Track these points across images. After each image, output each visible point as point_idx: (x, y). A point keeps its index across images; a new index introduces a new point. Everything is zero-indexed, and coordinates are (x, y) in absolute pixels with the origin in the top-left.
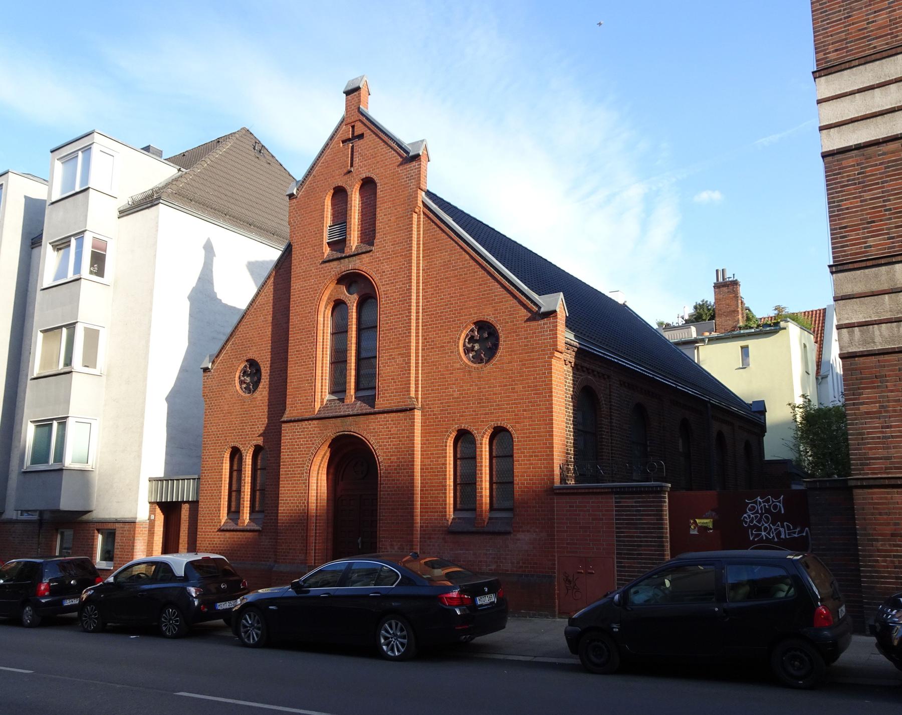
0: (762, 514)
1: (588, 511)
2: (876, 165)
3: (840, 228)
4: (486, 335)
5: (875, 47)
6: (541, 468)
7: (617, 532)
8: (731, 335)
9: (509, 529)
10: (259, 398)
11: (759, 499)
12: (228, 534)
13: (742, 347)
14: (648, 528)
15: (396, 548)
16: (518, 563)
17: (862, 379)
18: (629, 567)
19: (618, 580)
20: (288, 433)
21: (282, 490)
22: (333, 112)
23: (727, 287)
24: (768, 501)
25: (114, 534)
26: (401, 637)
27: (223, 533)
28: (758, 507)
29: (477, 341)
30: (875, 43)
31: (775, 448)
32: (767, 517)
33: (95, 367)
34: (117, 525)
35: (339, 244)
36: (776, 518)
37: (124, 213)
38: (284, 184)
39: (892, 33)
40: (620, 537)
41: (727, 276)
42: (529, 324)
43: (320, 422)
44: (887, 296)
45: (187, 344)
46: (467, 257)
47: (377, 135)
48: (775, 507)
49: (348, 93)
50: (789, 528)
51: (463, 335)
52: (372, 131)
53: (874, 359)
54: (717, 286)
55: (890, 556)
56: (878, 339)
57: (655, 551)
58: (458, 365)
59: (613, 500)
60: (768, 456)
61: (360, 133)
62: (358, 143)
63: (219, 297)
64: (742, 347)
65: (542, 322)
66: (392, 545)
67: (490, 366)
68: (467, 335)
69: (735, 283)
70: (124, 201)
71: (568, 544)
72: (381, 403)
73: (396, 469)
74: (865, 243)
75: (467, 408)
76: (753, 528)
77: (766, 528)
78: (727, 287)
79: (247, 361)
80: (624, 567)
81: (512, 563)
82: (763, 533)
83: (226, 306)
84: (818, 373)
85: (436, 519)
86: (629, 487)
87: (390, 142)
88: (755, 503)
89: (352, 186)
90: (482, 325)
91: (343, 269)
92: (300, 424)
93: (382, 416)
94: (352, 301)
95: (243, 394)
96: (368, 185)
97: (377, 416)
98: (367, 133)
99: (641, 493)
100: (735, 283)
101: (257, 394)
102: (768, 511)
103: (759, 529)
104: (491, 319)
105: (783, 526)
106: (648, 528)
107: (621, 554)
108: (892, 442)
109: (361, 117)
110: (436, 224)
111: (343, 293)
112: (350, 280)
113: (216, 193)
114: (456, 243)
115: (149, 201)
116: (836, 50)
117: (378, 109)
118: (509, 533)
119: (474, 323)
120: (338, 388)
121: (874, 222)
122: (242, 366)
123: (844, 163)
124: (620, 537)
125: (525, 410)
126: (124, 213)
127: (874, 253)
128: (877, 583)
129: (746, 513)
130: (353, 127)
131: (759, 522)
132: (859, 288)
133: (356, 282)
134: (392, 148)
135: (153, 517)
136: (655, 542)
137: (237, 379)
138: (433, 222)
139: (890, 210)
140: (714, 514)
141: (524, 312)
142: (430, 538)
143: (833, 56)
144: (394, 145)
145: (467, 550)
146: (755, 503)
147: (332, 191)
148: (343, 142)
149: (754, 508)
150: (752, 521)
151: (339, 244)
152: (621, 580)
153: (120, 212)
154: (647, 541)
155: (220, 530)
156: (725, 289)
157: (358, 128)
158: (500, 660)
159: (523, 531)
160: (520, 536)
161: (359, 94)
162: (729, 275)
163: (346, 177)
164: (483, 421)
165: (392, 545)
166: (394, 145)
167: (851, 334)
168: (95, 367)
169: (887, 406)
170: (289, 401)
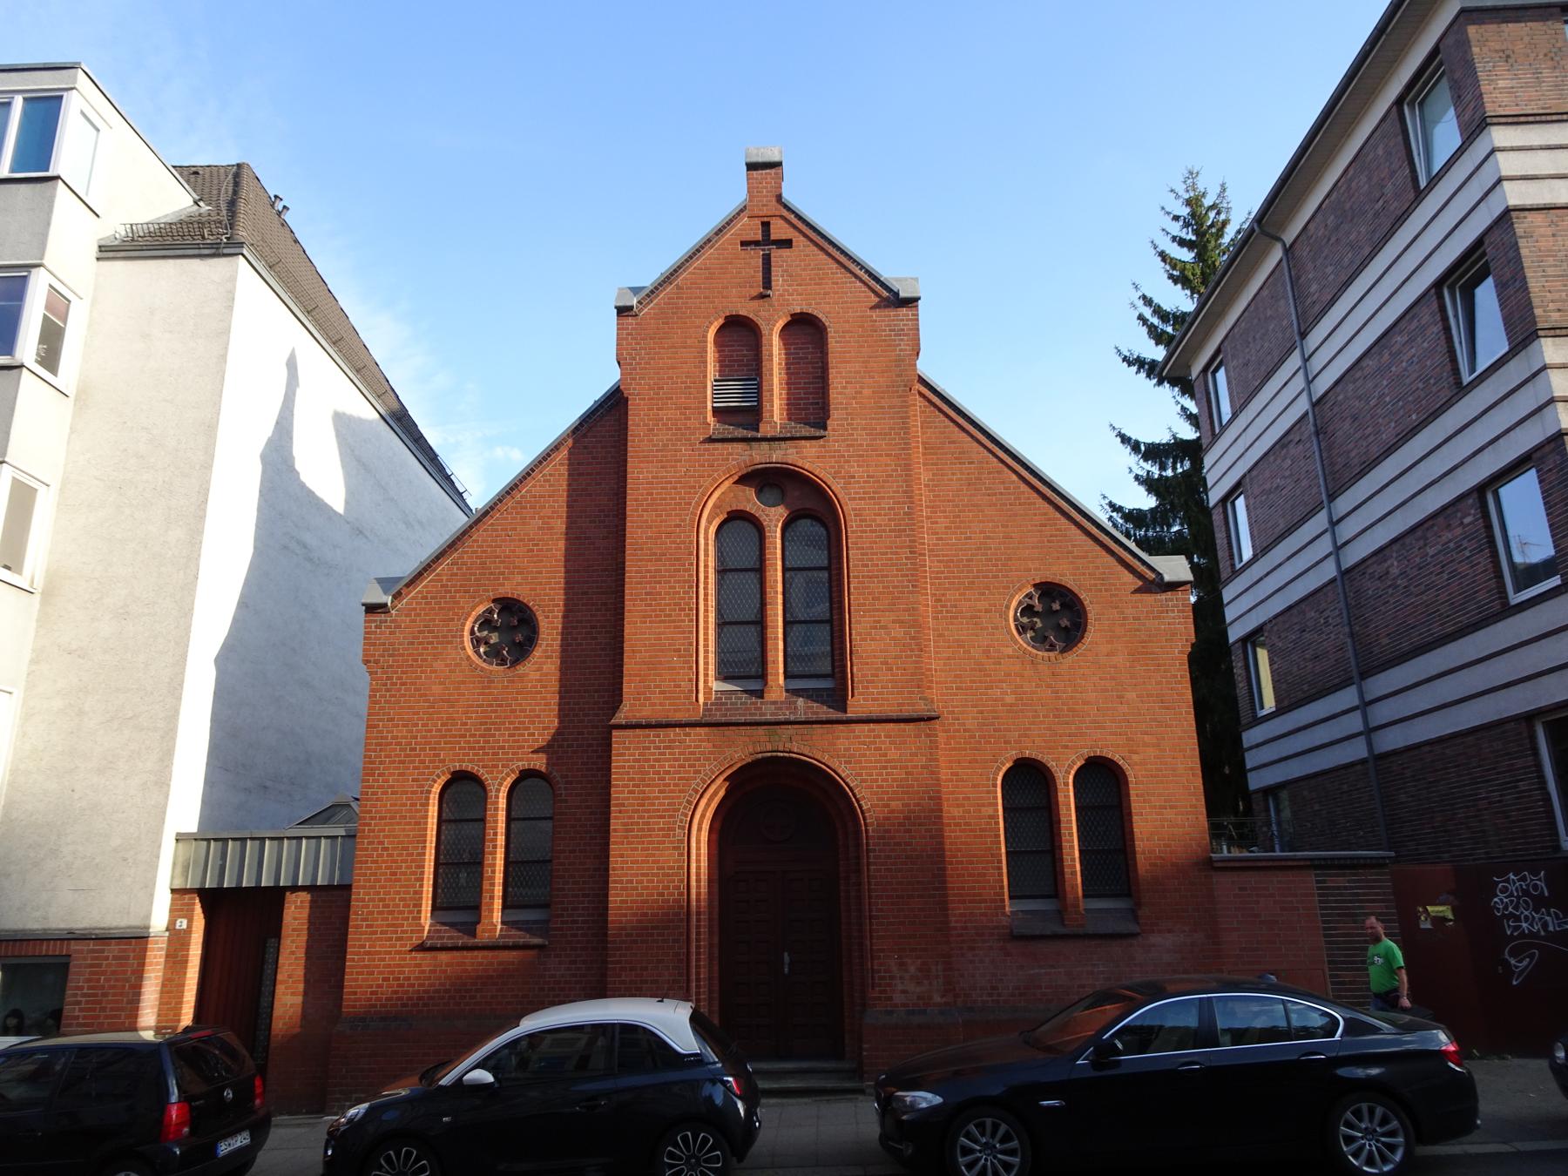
0: (1518, 898)
4: (1056, 606)
9: (1135, 928)
10: (534, 676)
12: (444, 957)
15: (912, 969)
18: (1351, 983)
20: (627, 751)
21: (615, 862)
22: (733, 192)
24: (1523, 879)
25: (66, 966)
26: (1004, 1152)
27: (428, 955)
29: (1037, 614)
33: (19, 572)
34: (74, 946)
35: (743, 418)
36: (1539, 903)
37: (108, 252)
42: (1138, 596)
43: (715, 730)
45: (251, 550)
46: (1014, 477)
47: (822, 249)
48: (1536, 887)
51: (1014, 604)
52: (811, 240)
58: (1009, 651)
59: (1310, 879)
62: (778, 255)
63: (298, 466)
65: (1163, 596)
66: (902, 965)
67: (1070, 658)
68: (1020, 603)
70: (114, 226)
72: (858, 704)
73: (900, 824)
77: (1527, 918)
79: (494, 601)
80: (1343, 983)
83: (303, 486)
85: (984, 915)
86: (1332, 859)
87: (852, 267)
88: (1507, 881)
89: (771, 322)
90: (1048, 590)
91: (758, 459)
92: (662, 732)
93: (866, 727)
94: (774, 518)
95: (484, 665)
96: (805, 328)
97: (853, 726)
98: (799, 240)
99: (1364, 866)
101: (527, 668)
102: (1526, 893)
103: (1517, 919)
104: (1069, 581)
109: (785, 213)
110: (947, 416)
111: (749, 500)
112: (767, 480)
114: (990, 451)
118: (1133, 935)
119: (1035, 586)
120: (742, 666)
122: (481, 609)
126: (108, 252)
128: (698, 894)
131: (1516, 908)
134: (856, 276)
135: (182, 924)
137: (466, 633)
138: (940, 410)
140: (1451, 898)
141: (1128, 577)
142: (973, 949)
144: (861, 273)
145: (1052, 967)
146: (1507, 881)
147: (721, 321)
148: (743, 244)
150: (1506, 908)
151: (743, 418)
153: (101, 248)
155: (422, 948)
157: (770, 230)
160: (1155, 939)
163: (756, 303)
164: (1066, 747)
166: (861, 273)
168: (19, 572)
170: (628, 688)
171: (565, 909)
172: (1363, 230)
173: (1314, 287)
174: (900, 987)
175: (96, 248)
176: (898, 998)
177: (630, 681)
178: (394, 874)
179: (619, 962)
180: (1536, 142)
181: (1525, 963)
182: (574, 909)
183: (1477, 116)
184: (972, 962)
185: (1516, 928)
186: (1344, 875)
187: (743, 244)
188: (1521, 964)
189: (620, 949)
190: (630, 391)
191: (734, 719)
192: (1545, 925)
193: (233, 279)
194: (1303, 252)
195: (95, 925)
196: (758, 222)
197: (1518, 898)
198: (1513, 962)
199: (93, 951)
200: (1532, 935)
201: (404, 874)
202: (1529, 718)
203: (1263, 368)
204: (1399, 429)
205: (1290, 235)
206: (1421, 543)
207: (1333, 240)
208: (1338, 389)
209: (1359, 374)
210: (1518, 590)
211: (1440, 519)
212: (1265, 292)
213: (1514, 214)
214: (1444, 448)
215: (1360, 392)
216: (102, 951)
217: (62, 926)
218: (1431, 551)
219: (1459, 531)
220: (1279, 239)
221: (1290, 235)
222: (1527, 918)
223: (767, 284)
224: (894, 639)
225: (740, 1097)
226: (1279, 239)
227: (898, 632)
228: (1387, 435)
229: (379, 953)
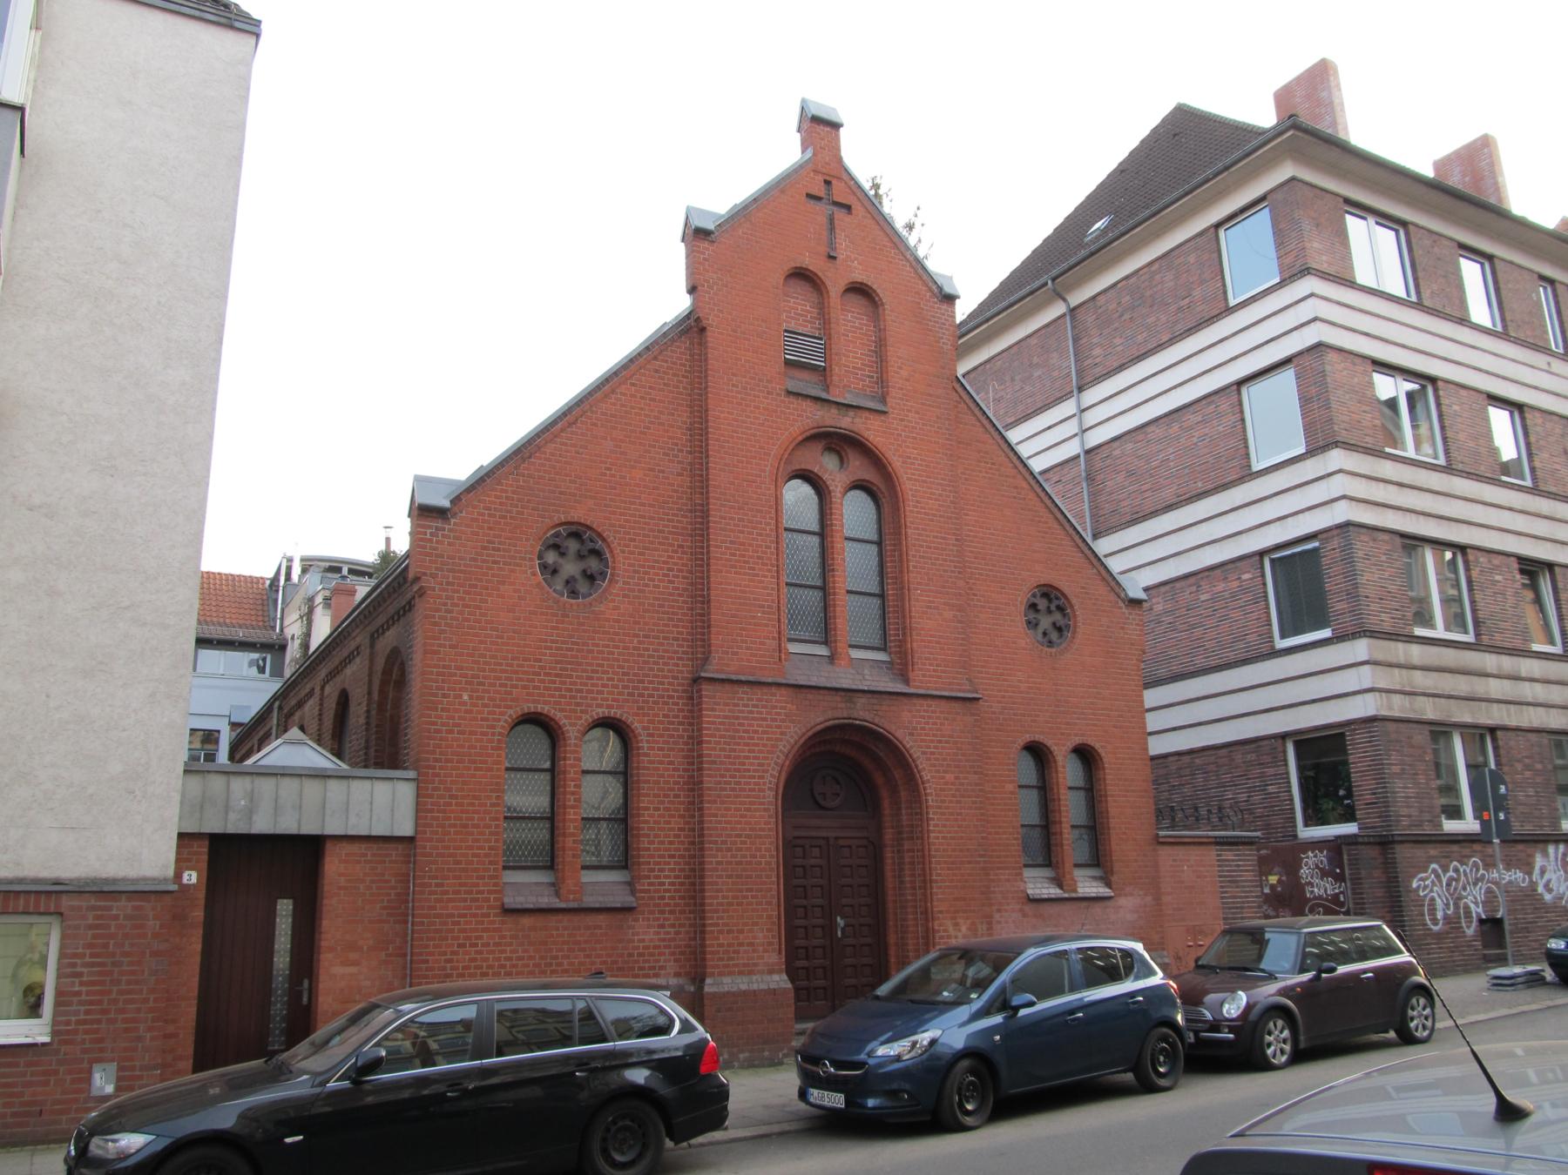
15: (964, 929)
59: (1211, 854)
142: (999, 911)
160: (1122, 901)
165: (957, 924)
171: (653, 870)
172: (1163, 318)
173: (1097, 351)
177: (718, 633)
178: (466, 826)
179: (717, 925)
180: (1335, 297)
182: (661, 870)
183: (1299, 263)
187: (808, 195)
189: (717, 911)
190: (711, 321)
191: (763, 680)
194: (1089, 318)
195: (92, 874)
196: (820, 178)
199: (93, 908)
200: (1320, 897)
201: (478, 826)
202: (1283, 737)
203: (1021, 408)
204: (1180, 491)
205: (1076, 298)
206: (1194, 589)
207: (1127, 316)
208: (1117, 444)
209: (1140, 437)
210: (1283, 637)
211: (1218, 572)
212: (1034, 341)
213: (1331, 356)
215: (1140, 453)
216: (109, 908)
217: (45, 874)
218: (1203, 598)
219: (1236, 584)
220: (1064, 300)
221: (1076, 298)
225: (1317, 978)
226: (1064, 300)
227: (948, 614)
228: (1168, 494)
229: (452, 915)
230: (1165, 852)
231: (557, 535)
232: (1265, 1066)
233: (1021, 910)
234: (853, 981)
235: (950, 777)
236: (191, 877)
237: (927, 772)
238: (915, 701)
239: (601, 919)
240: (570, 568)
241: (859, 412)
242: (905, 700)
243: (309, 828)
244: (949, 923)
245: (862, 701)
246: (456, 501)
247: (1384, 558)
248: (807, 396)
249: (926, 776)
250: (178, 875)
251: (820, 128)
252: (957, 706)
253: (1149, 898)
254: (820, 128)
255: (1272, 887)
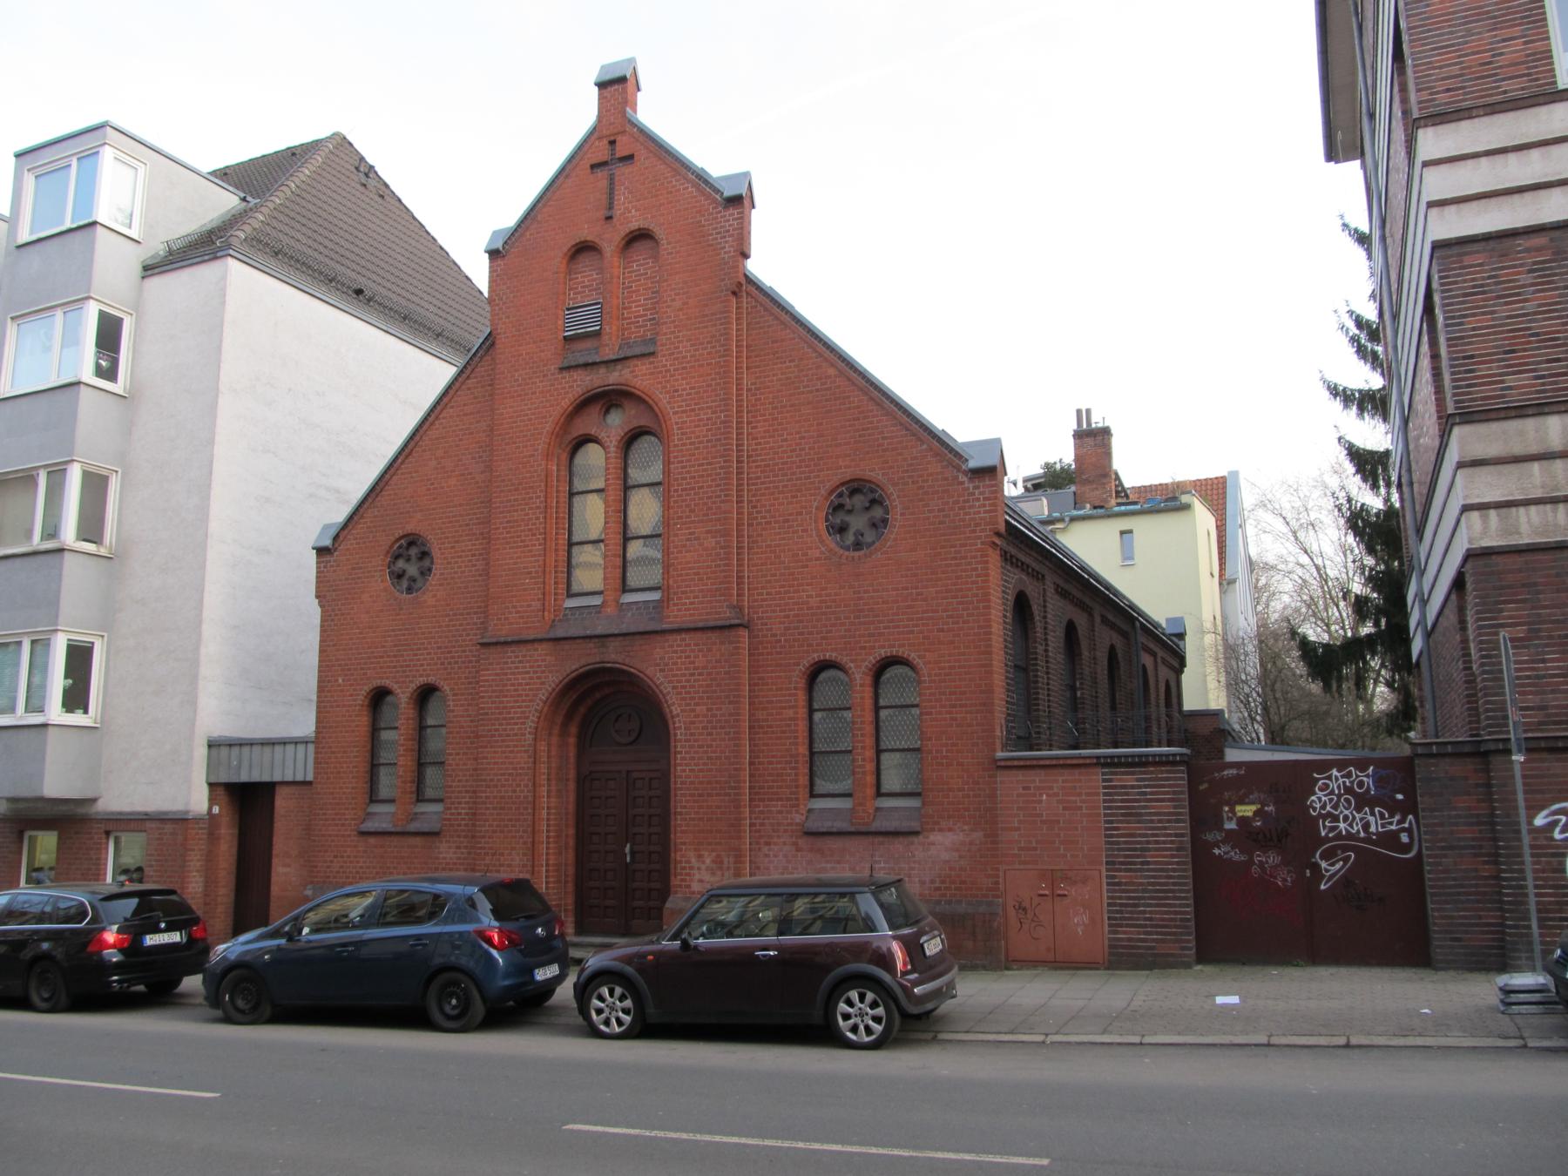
1: (1057, 795)
2: (1515, 266)
3: (1465, 358)
5: (1505, 92)
6: (970, 725)
7: (1107, 829)
8: (1101, 512)
9: (915, 825)
11: (1334, 772)
13: (1122, 533)
14: (1160, 821)
15: (708, 861)
16: (932, 882)
17: (1502, 588)
19: (1109, 905)
23: (1093, 440)
24: (1349, 775)
28: (1333, 785)
30: (1505, 85)
31: (1203, 688)
32: (1347, 800)
36: (1363, 801)
38: (275, 223)
39: (1529, 75)
40: (1112, 836)
41: (1094, 419)
44: (1536, 466)
48: (1361, 784)
49: (602, 85)
50: (1382, 816)
53: (1520, 560)
54: (1079, 436)
55: (1545, 855)
56: (1524, 528)
57: (1173, 856)
58: (815, 553)
59: (1097, 777)
60: (1190, 703)
61: (626, 153)
62: (623, 171)
64: (1122, 533)
66: (700, 856)
69: (1105, 433)
71: (1020, 849)
74: (1502, 382)
75: (834, 625)
76: (1325, 817)
77: (1346, 818)
78: (1093, 440)
80: (1119, 884)
81: (922, 883)
82: (1342, 825)
84: (1221, 576)
88: (1329, 778)
91: (597, 383)
100: (1105, 433)
102: (1349, 790)
103: (1336, 819)
105: (1373, 814)
106: (1160, 821)
107: (1113, 863)
108: (1548, 684)
113: (310, 242)
115: (205, 246)
116: (1448, 90)
117: (650, 112)
118: (916, 833)
121: (1513, 351)
123: (1467, 260)
124: (1112, 836)
125: (942, 630)
127: (1515, 399)
129: (1314, 793)
130: (612, 143)
131: (1335, 807)
132: (1493, 451)
133: (617, 406)
136: (1172, 842)
139: (1537, 335)
142: (768, 844)
143: (1442, 98)
146: (1329, 778)
149: (1327, 786)
150: (1323, 807)
152: (1115, 905)
154: (1157, 842)
156: (1090, 441)
157: (618, 148)
158: (950, 1041)
159: (941, 830)
160: (935, 837)
161: (625, 91)
162: (1097, 421)
165: (700, 856)
167: (1485, 519)
169: (1539, 630)
174: (697, 877)
175: (140, 268)
176: (696, 887)
181: (1338, 866)
184: (767, 856)
185: (1332, 829)
186: (1133, 773)
187: (593, 167)
188: (1332, 869)
192: (1366, 826)
193: (224, 278)
196: (605, 142)
197: (1339, 796)
198: (1324, 864)
200: (1350, 836)
214: (18, 561)
222: (1346, 818)
223: (611, 207)
224: (706, 549)
227: (710, 542)
230: (1002, 777)
231: (840, 495)
232: (825, 1035)
233: (795, 844)
234: (640, 903)
235: (701, 709)
236: (216, 810)
237: (675, 707)
238: (671, 637)
239: (418, 840)
240: (412, 570)
241: (627, 363)
242: (658, 638)
243: (266, 778)
244: (691, 854)
245: (613, 645)
246: (336, 538)
247: (1526, 279)
248: (577, 366)
249: (676, 710)
250: (210, 809)
251: (616, 87)
252: (713, 636)
253: (978, 836)
254: (616, 87)
255: (1243, 821)
